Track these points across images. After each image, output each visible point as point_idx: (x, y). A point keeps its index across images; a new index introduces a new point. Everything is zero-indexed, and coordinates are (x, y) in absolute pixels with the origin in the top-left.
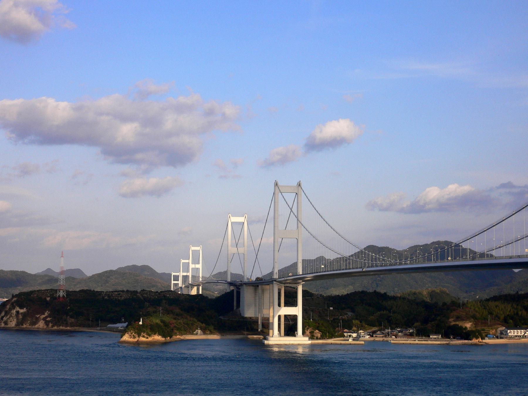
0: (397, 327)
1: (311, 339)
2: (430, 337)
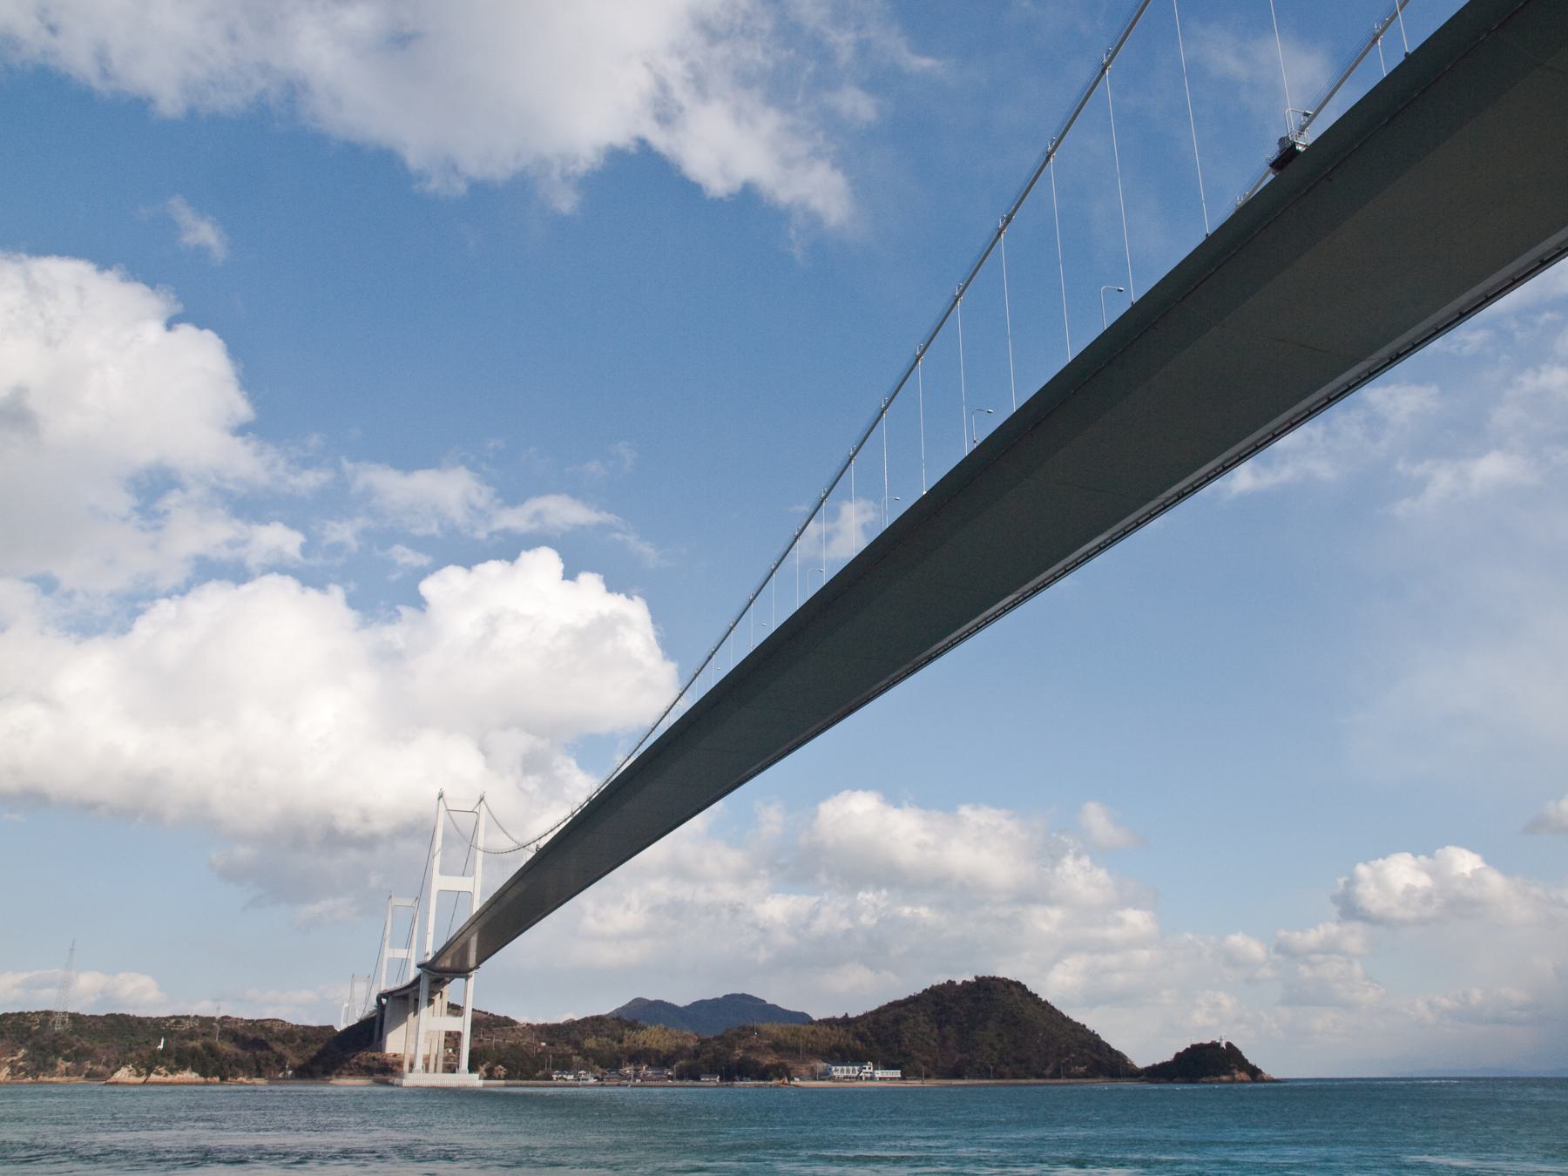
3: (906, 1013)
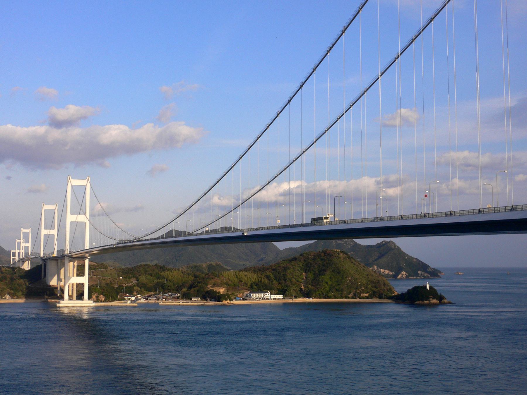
0: (169, 292)
1: (94, 302)
2: (191, 299)
3: (290, 266)
